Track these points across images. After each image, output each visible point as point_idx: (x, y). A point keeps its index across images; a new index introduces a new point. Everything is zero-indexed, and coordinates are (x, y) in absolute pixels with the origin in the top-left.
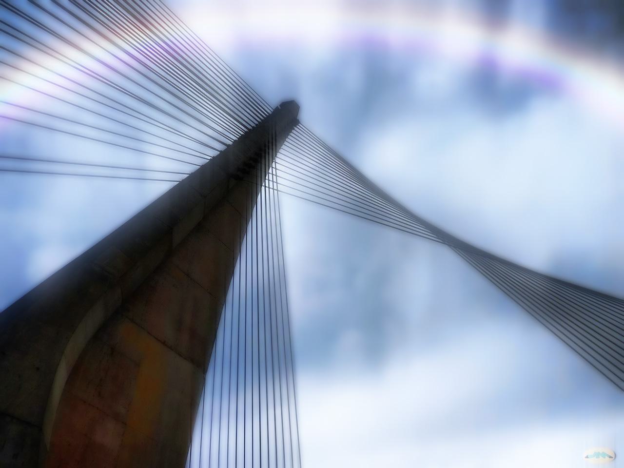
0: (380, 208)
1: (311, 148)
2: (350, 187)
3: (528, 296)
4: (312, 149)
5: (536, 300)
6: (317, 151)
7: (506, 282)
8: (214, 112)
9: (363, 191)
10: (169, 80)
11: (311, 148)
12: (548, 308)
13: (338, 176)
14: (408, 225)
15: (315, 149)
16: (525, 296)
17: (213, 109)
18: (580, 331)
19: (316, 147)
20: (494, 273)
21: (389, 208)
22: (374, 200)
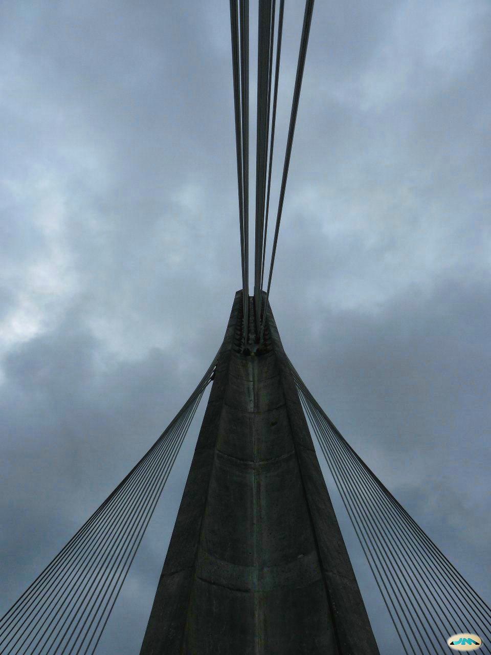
0: (130, 537)
1: (144, 497)
2: (150, 498)
3: (363, 500)
4: (119, 519)
5: (375, 504)
6: (63, 556)
7: (342, 476)
8: (346, 458)
9: (65, 559)
10: (446, 559)
11: (144, 497)
12: (366, 503)
13: (73, 566)
14: (364, 511)
15: (58, 562)
16: (422, 540)
17: (360, 485)
18: (403, 562)
19: (131, 503)
20: (347, 485)
21: (166, 459)
22: (146, 476)
